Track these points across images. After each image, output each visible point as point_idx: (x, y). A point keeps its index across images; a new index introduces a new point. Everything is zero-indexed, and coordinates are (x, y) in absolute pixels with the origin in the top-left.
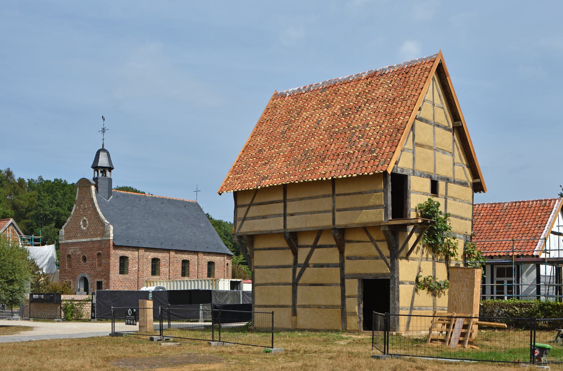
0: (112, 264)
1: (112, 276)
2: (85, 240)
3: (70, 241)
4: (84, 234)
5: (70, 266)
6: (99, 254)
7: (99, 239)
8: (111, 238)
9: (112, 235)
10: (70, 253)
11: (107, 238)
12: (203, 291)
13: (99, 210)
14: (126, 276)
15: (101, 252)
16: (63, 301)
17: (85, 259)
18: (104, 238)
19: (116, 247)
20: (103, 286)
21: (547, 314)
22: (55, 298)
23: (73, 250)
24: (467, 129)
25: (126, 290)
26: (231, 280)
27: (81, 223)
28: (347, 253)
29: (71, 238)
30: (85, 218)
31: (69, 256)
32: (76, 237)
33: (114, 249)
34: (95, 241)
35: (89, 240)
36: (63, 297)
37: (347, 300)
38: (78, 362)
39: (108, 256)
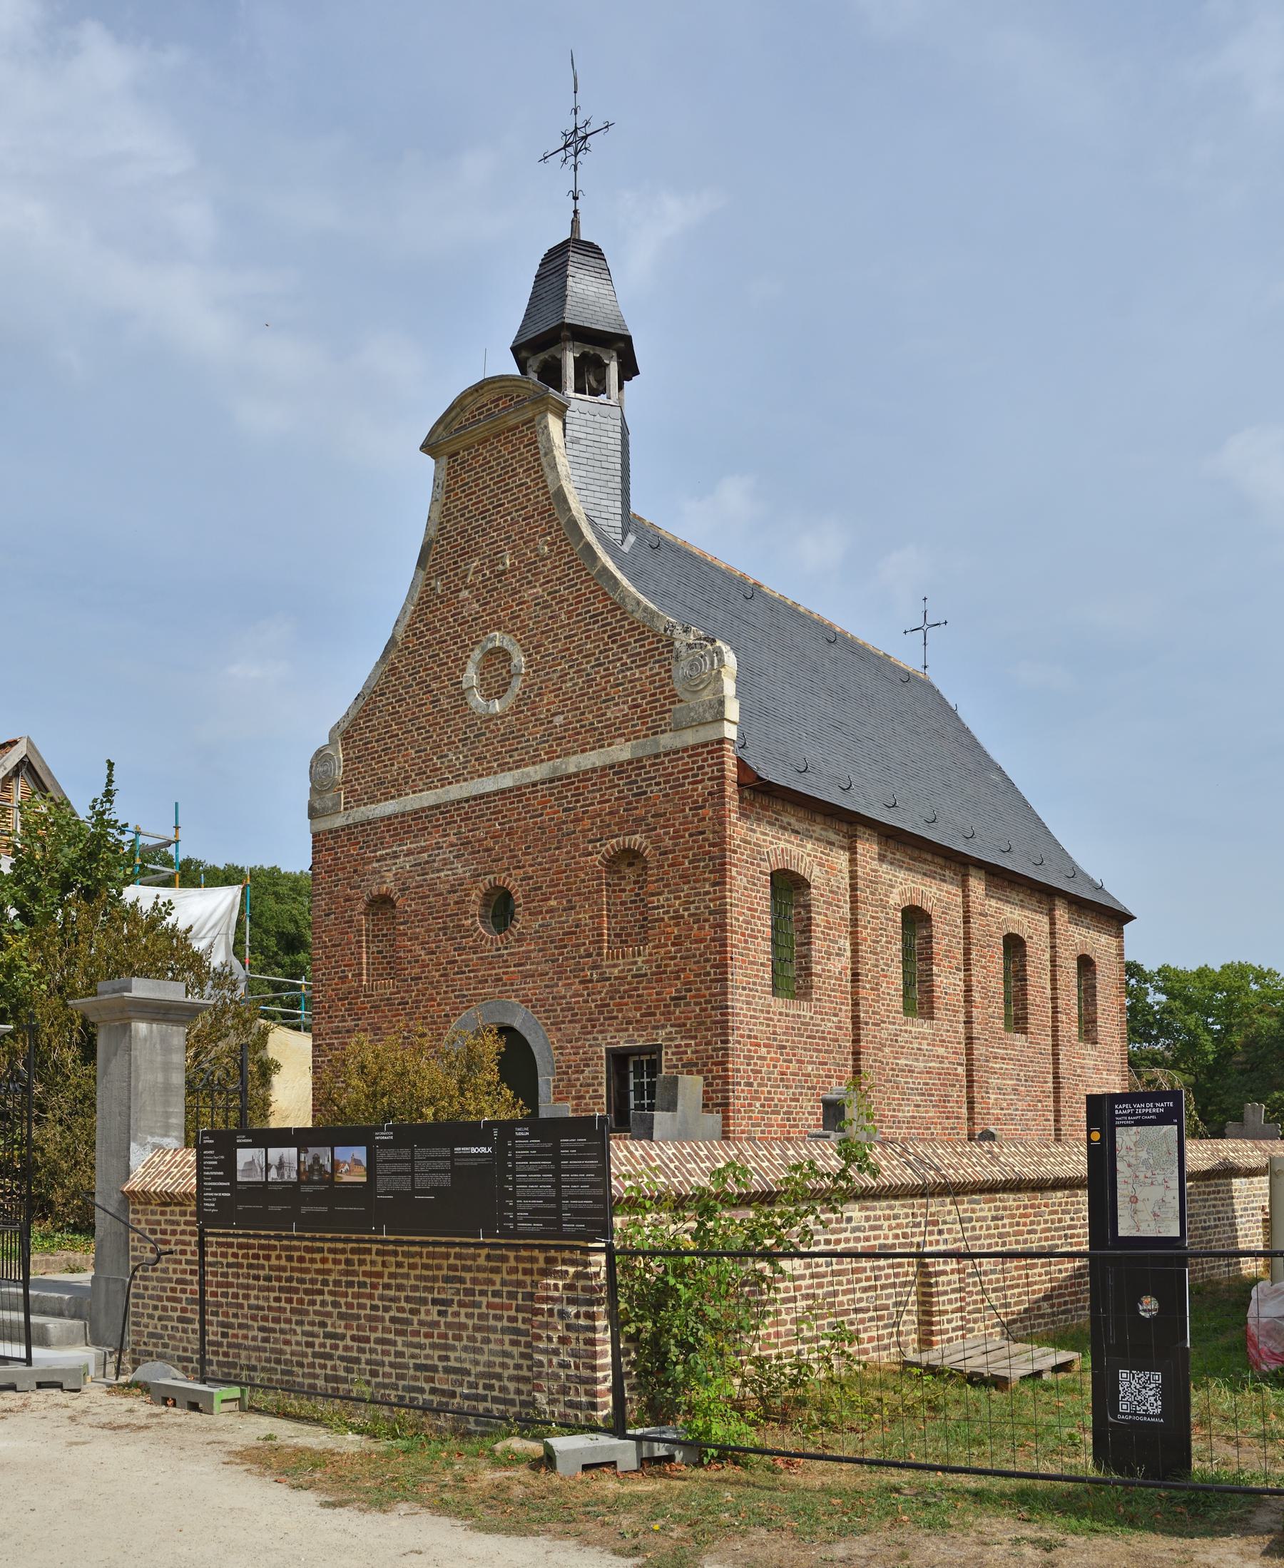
0: (736, 918)
1: (738, 1001)
2: (506, 780)
3: (388, 808)
4: (503, 745)
5: (389, 965)
6: (631, 856)
7: (621, 751)
8: (730, 732)
9: (732, 710)
10: (389, 885)
11: (690, 738)
12: (1189, 1436)
13: (488, 785)
14: (804, 1010)
15: (637, 839)
16: (633, 1205)
17: (500, 908)
18: (667, 741)
19: (763, 794)
20: (993, 903)
21: (1166, 979)
22: (530, 1184)
23: (406, 863)
24: (50, 773)
25: (612, 330)
26: (570, 391)
27: (471, 676)
28: (1070, 1219)
29: (395, 789)
30: (498, 639)
31: (382, 903)
32: (431, 776)
33: (744, 815)
34: (584, 776)
35: (536, 772)
36: (630, 1162)
37: (1075, 1163)
38: (859, 1546)
39: (715, 862)
